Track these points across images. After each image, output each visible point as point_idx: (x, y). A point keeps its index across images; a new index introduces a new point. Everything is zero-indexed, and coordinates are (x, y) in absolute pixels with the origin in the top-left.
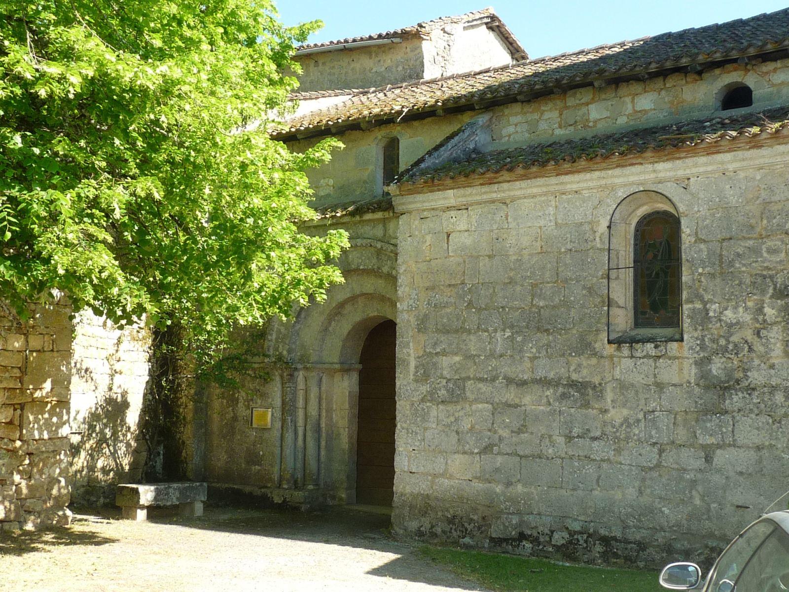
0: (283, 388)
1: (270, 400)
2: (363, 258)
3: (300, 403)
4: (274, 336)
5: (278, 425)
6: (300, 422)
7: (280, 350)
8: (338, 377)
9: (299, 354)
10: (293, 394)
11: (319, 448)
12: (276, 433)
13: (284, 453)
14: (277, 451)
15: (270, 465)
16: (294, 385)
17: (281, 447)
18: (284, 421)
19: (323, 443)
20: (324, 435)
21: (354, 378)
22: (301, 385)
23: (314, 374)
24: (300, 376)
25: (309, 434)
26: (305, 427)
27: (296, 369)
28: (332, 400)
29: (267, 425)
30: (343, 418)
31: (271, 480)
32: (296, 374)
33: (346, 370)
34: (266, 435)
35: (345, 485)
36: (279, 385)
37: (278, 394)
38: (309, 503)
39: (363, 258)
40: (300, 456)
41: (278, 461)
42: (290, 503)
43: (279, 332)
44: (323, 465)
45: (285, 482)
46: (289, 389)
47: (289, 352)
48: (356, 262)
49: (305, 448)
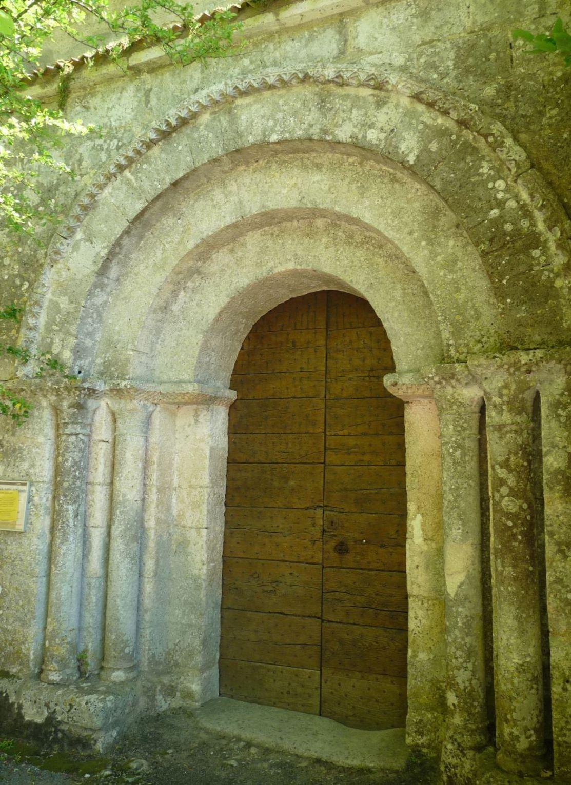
0: (58, 436)
1: (25, 465)
2: (280, 116)
3: (99, 472)
4: (43, 320)
5: (43, 523)
6: (98, 517)
7: (56, 350)
8: (185, 416)
9: (99, 361)
10: (81, 451)
11: (140, 575)
12: (37, 544)
13: (53, 595)
14: (37, 587)
15: (18, 619)
16: (87, 431)
17: (48, 575)
18: (56, 516)
19: (150, 564)
20: (152, 545)
21: (220, 423)
22: (102, 430)
23: (136, 404)
24: (101, 409)
25: (118, 545)
26: (109, 527)
27: (92, 392)
28: (170, 466)
29: (14, 523)
30: (196, 505)
31: (19, 657)
32: (91, 404)
33: (207, 401)
34: (12, 548)
35: (199, 659)
36: (49, 431)
37: (47, 450)
38: (116, 724)
39: (280, 116)
40: (94, 597)
41: (39, 611)
42: (64, 727)
43: (55, 306)
44: (147, 617)
45: (53, 666)
46: (72, 439)
47: (78, 352)
48: (258, 130)
49: (106, 576)
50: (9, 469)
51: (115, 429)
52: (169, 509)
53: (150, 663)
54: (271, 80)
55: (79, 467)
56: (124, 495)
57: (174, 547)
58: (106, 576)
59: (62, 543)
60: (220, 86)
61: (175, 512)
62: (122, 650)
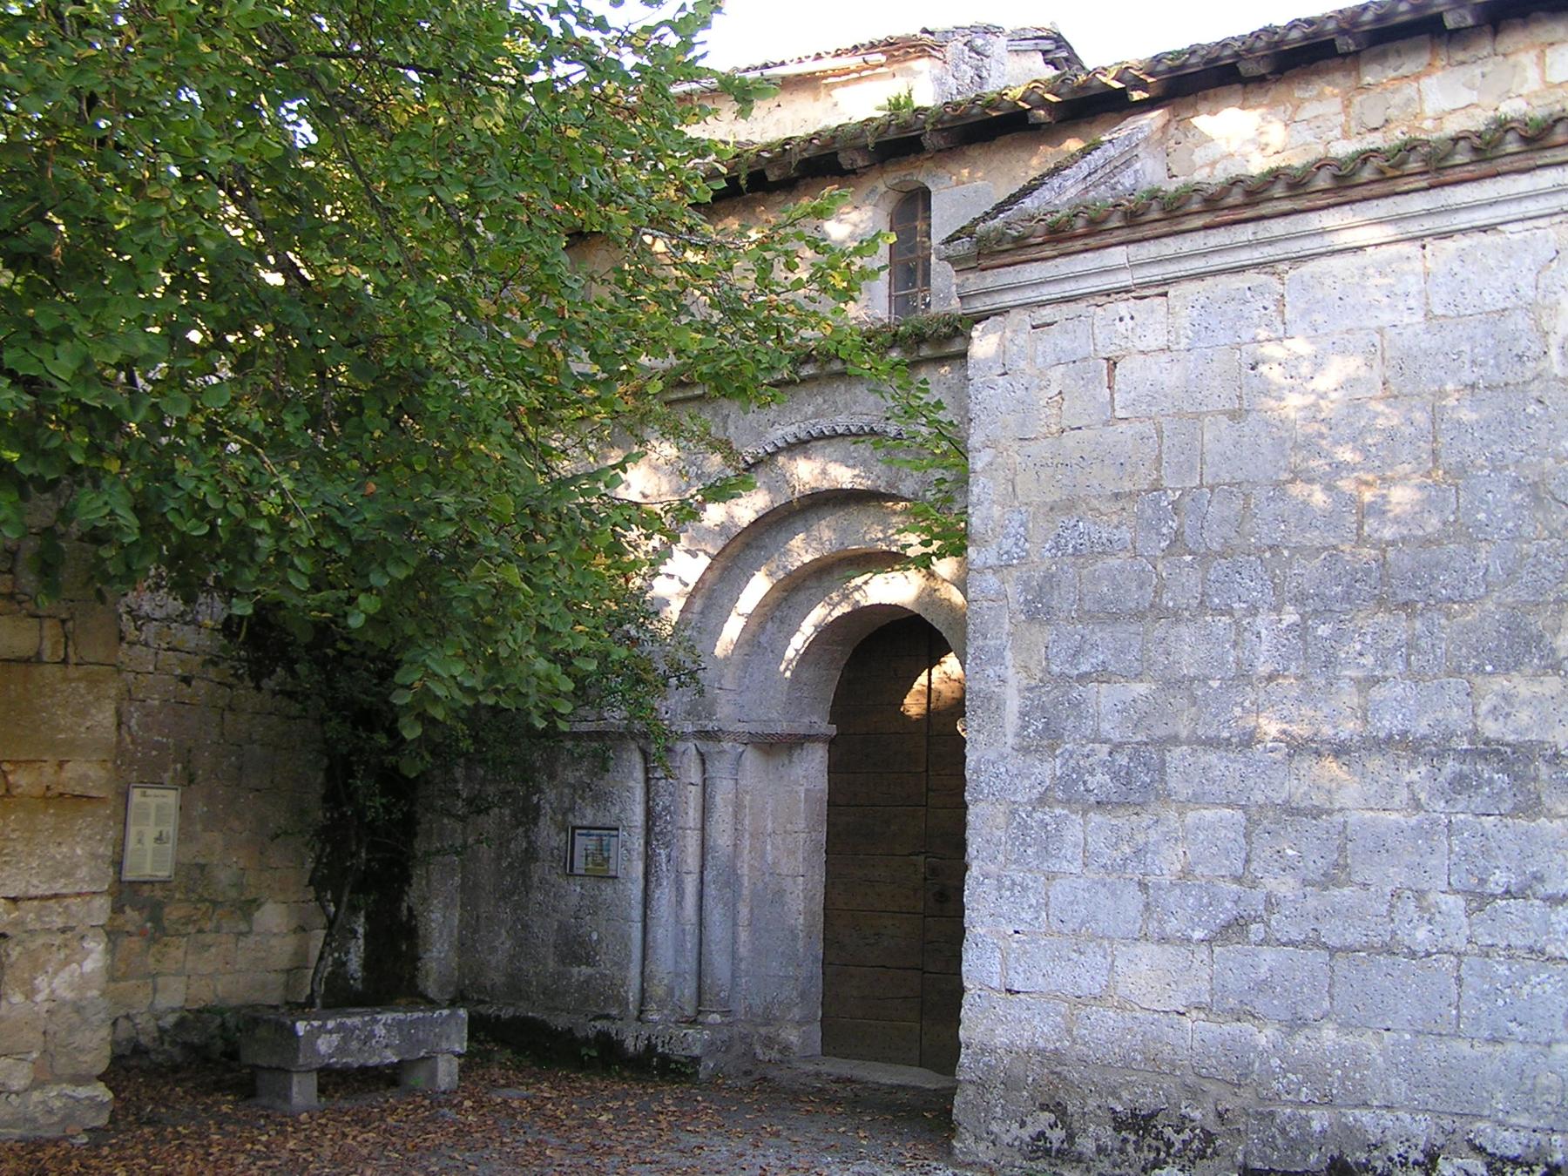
6: (692, 863)
11: (735, 924)
13: (650, 937)
19: (744, 911)
40: (690, 943)
49: (701, 923)
50: (600, 814)
51: (704, 772)
52: (763, 856)
53: (746, 1012)
54: (840, 430)
55: (670, 812)
56: (715, 841)
57: (770, 896)
58: (701, 923)
59: (656, 887)
60: (794, 429)
61: (770, 859)
62: (718, 995)
